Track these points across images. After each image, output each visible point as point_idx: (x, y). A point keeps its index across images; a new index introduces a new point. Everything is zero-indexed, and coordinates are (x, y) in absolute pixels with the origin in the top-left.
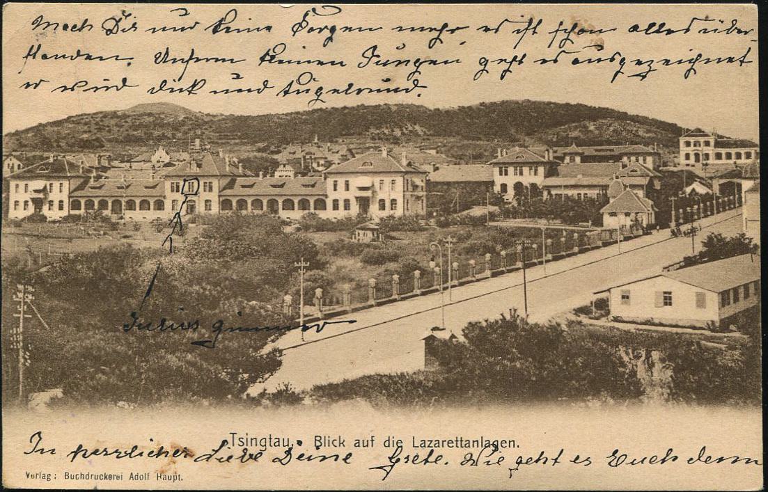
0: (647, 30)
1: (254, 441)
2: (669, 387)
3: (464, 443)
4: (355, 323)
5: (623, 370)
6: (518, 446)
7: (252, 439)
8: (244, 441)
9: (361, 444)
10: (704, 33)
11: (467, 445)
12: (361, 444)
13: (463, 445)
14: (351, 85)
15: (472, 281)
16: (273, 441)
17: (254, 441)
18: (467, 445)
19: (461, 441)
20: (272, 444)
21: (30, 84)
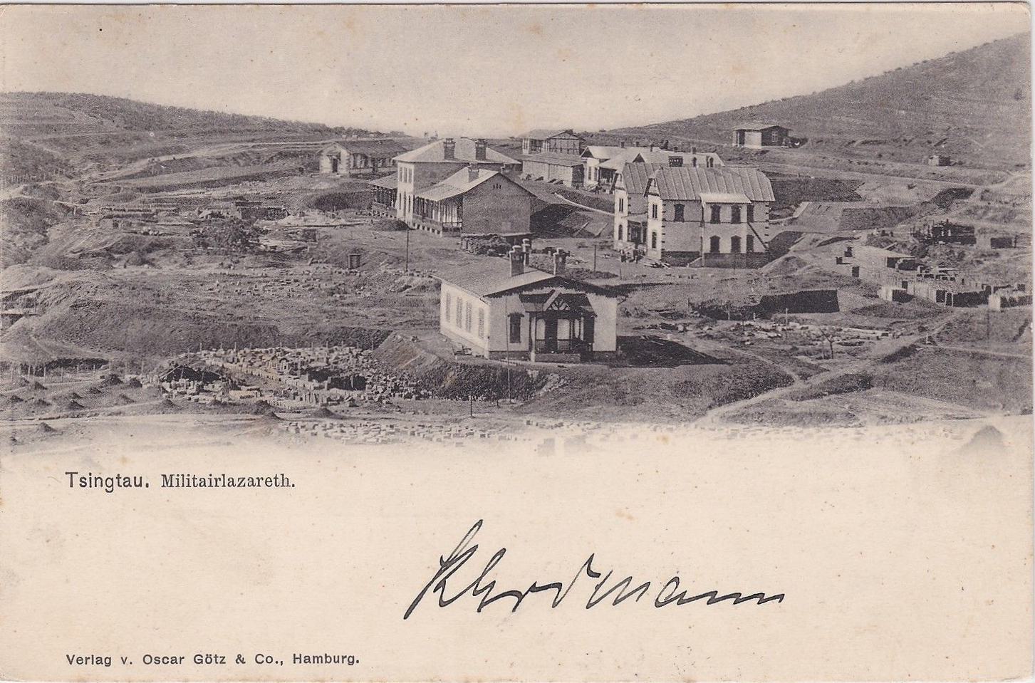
6: (147, 485)
8: (88, 481)
11: (127, 484)
12: (132, 483)
13: (121, 484)
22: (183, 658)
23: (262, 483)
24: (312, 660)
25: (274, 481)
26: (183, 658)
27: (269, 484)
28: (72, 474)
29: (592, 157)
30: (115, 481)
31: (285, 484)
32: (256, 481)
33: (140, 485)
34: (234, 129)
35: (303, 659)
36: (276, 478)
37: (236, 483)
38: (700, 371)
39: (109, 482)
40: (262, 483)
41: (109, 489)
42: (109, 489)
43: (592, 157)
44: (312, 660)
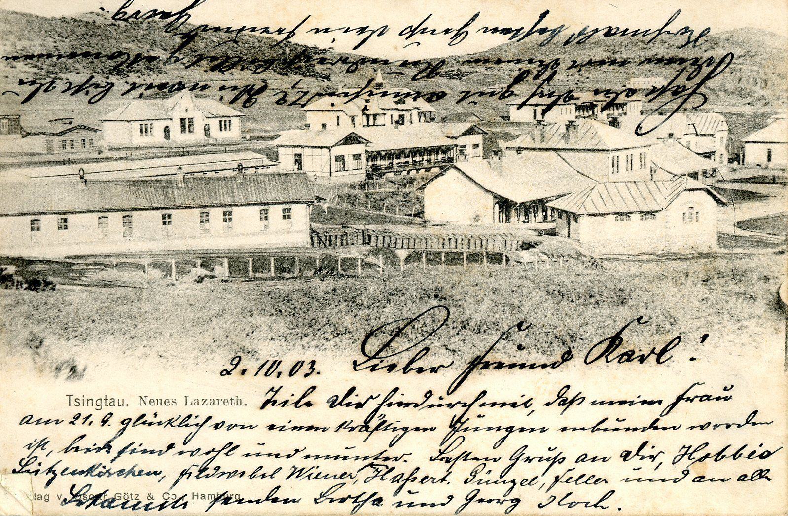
0: (577, 481)
1: (90, 402)
2: (752, 34)
3: (108, 402)
4: (261, 405)
5: (317, 261)
6: (127, 405)
7: (88, 400)
8: (81, 402)
9: (116, 404)
10: (58, 420)
11: (112, 404)
12: (116, 404)
13: (108, 404)
14: (101, 464)
15: (149, 148)
16: (108, 402)
17: (90, 402)
18: (112, 404)
19: (106, 399)
20: (108, 404)
21: (699, 428)
22: (606, 482)
23: (221, 403)
24: (206, 497)
25: (230, 401)
26: (606, 482)
27: (226, 404)
28: (70, 396)
29: (495, 196)
30: (103, 402)
31: (239, 403)
32: (216, 402)
33: (123, 405)
34: (485, 89)
35: (200, 497)
36: (231, 399)
37: (201, 403)
38: (333, 321)
39: (99, 403)
40: (221, 403)
41: (99, 408)
42: (99, 408)
43: (495, 196)
44: (206, 497)
